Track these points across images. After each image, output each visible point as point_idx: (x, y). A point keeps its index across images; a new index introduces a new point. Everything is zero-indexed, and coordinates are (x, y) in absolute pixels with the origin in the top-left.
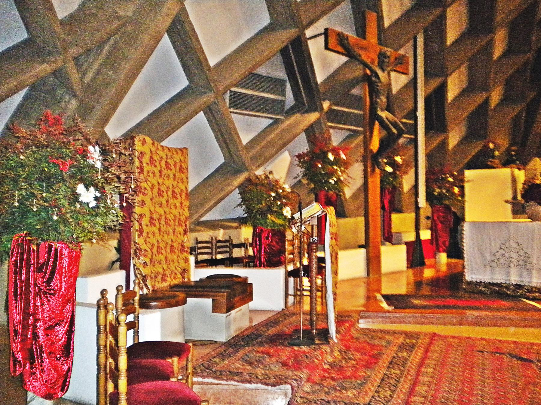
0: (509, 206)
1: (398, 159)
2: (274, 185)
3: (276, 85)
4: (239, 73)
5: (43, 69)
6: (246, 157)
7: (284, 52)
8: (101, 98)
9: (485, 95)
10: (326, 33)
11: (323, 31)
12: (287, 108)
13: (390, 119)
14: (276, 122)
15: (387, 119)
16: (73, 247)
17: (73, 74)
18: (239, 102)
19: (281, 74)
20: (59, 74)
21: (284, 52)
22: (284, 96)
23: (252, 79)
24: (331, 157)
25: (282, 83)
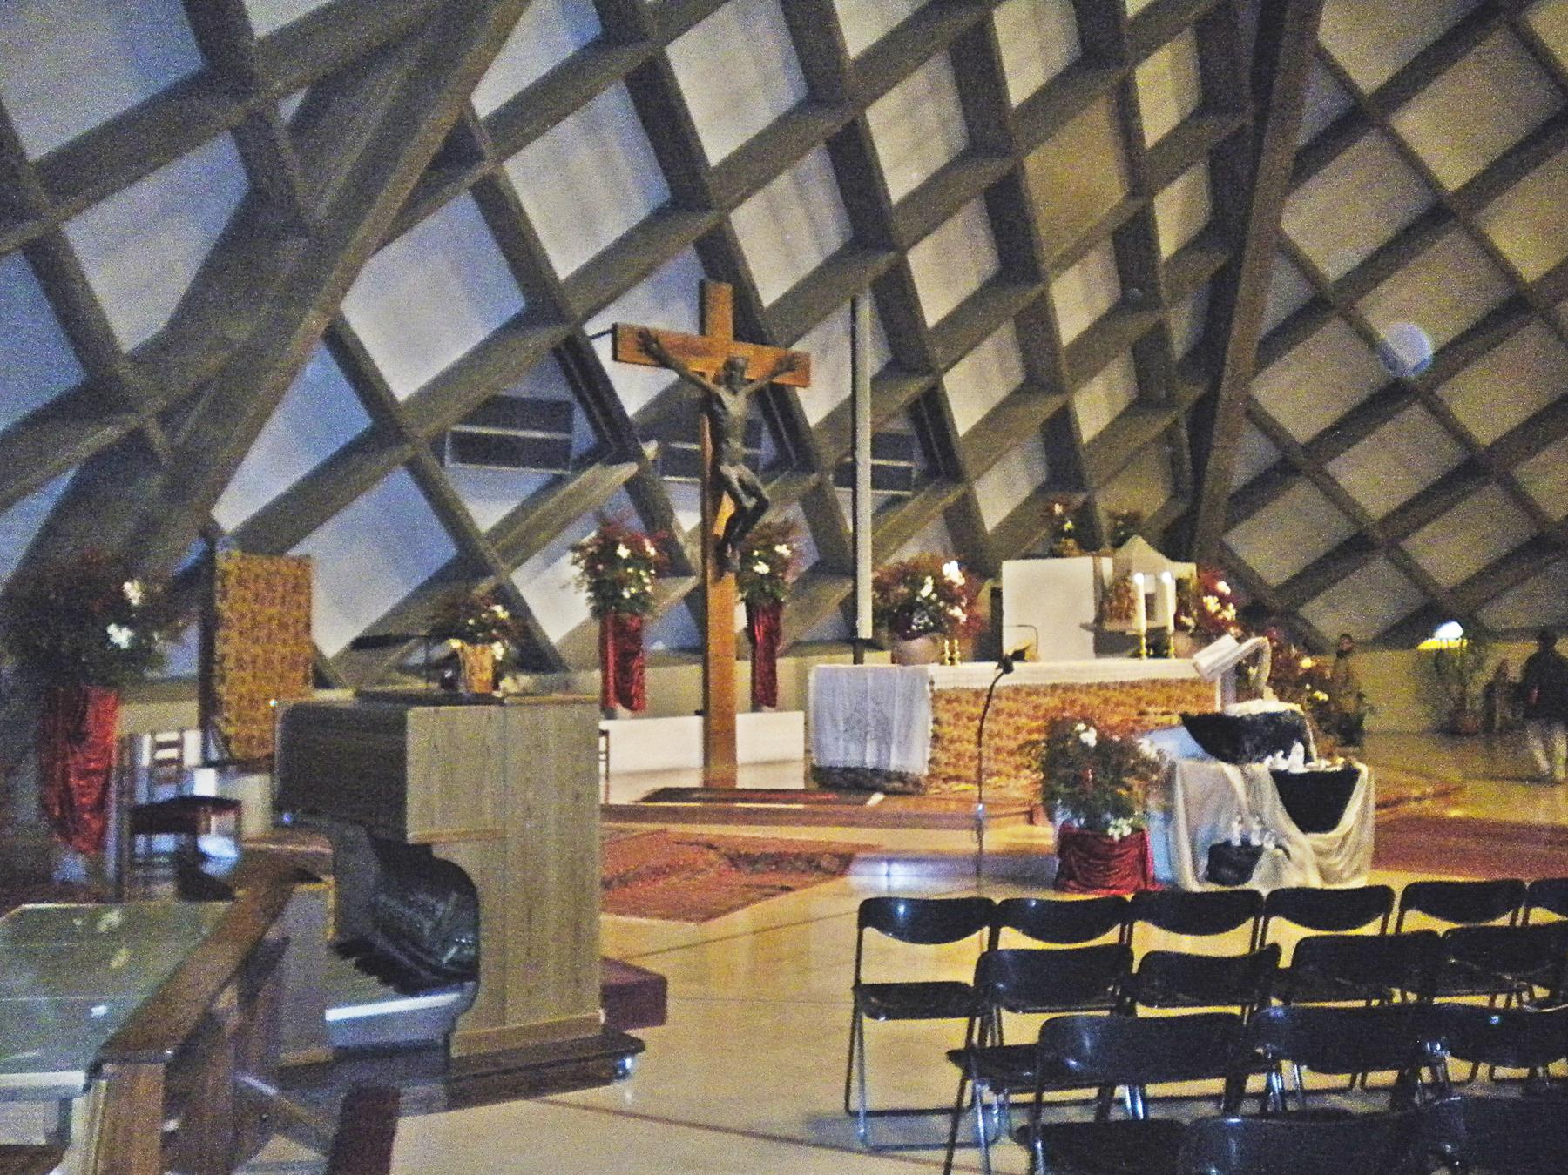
0: (1090, 636)
1: (782, 549)
2: (1532, 661)
3: (555, 414)
4: (458, 408)
5: (110, 433)
6: (492, 554)
7: (556, 352)
8: (199, 476)
9: (1055, 402)
10: (614, 330)
11: (609, 327)
12: (574, 455)
13: (746, 479)
14: (559, 481)
15: (740, 480)
16: (119, 1140)
17: (157, 436)
18: (473, 450)
19: (559, 391)
20: (136, 442)
21: (556, 352)
22: (569, 430)
23: (496, 408)
24: (623, 552)
25: (569, 407)
